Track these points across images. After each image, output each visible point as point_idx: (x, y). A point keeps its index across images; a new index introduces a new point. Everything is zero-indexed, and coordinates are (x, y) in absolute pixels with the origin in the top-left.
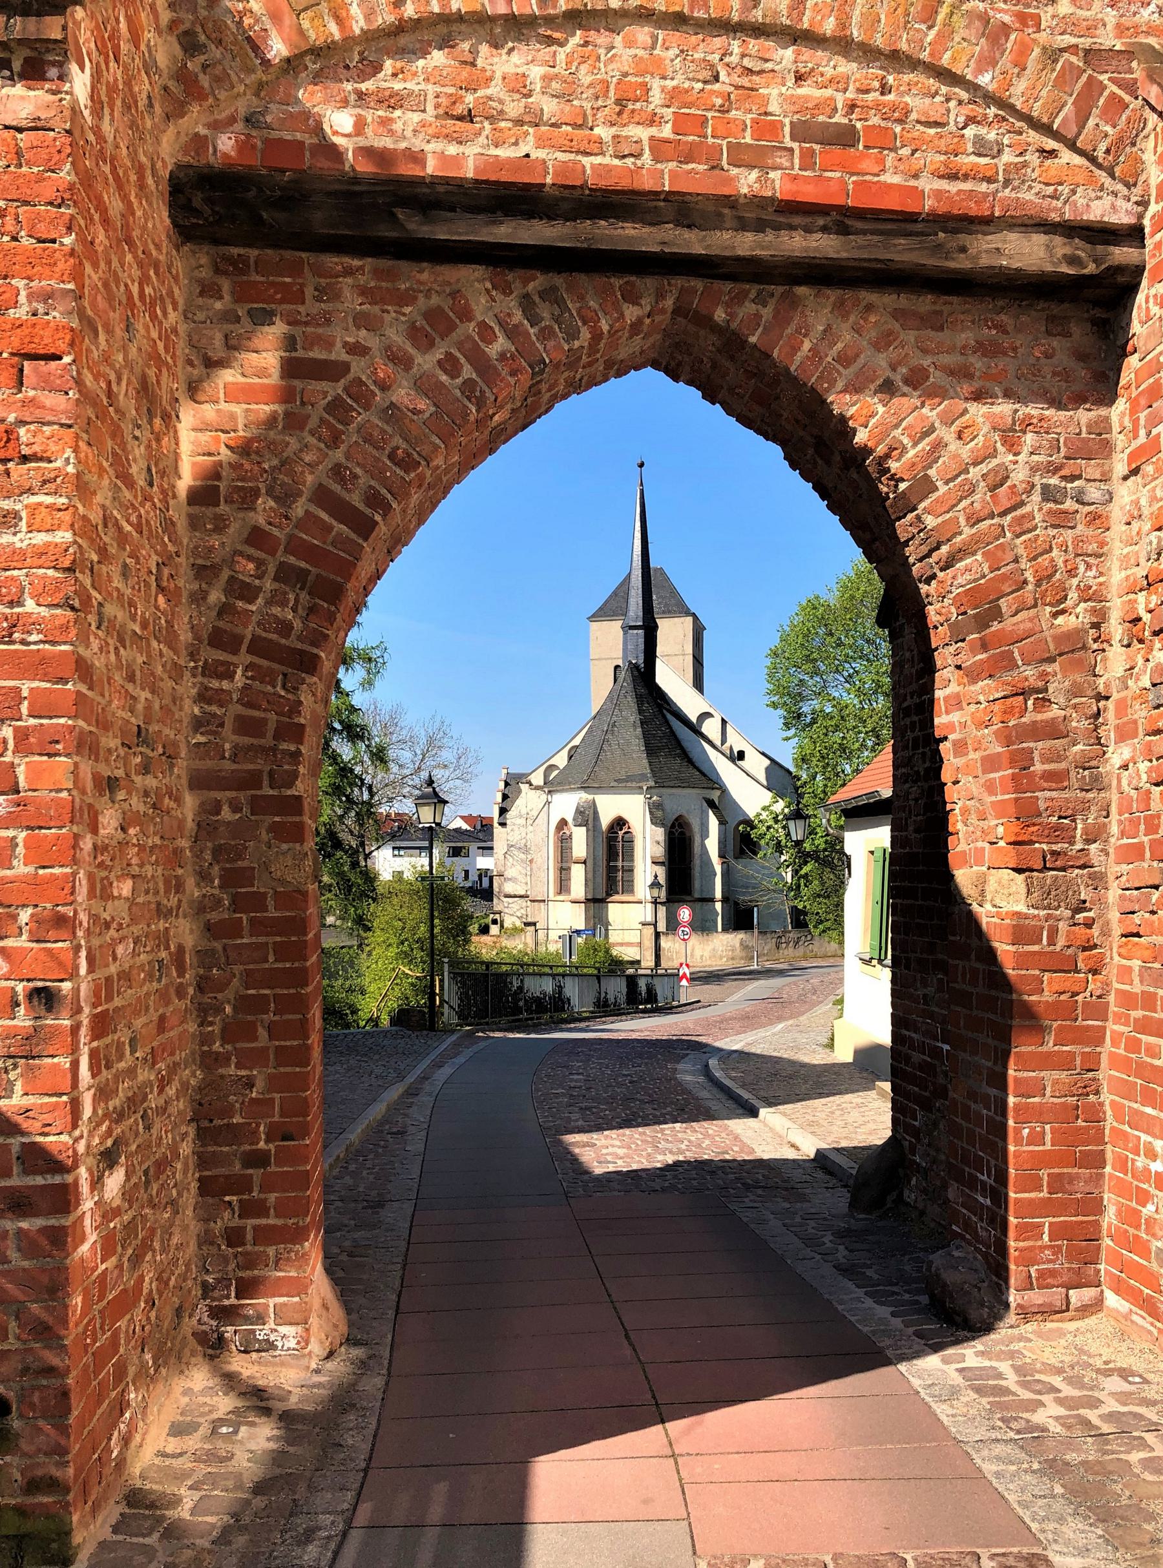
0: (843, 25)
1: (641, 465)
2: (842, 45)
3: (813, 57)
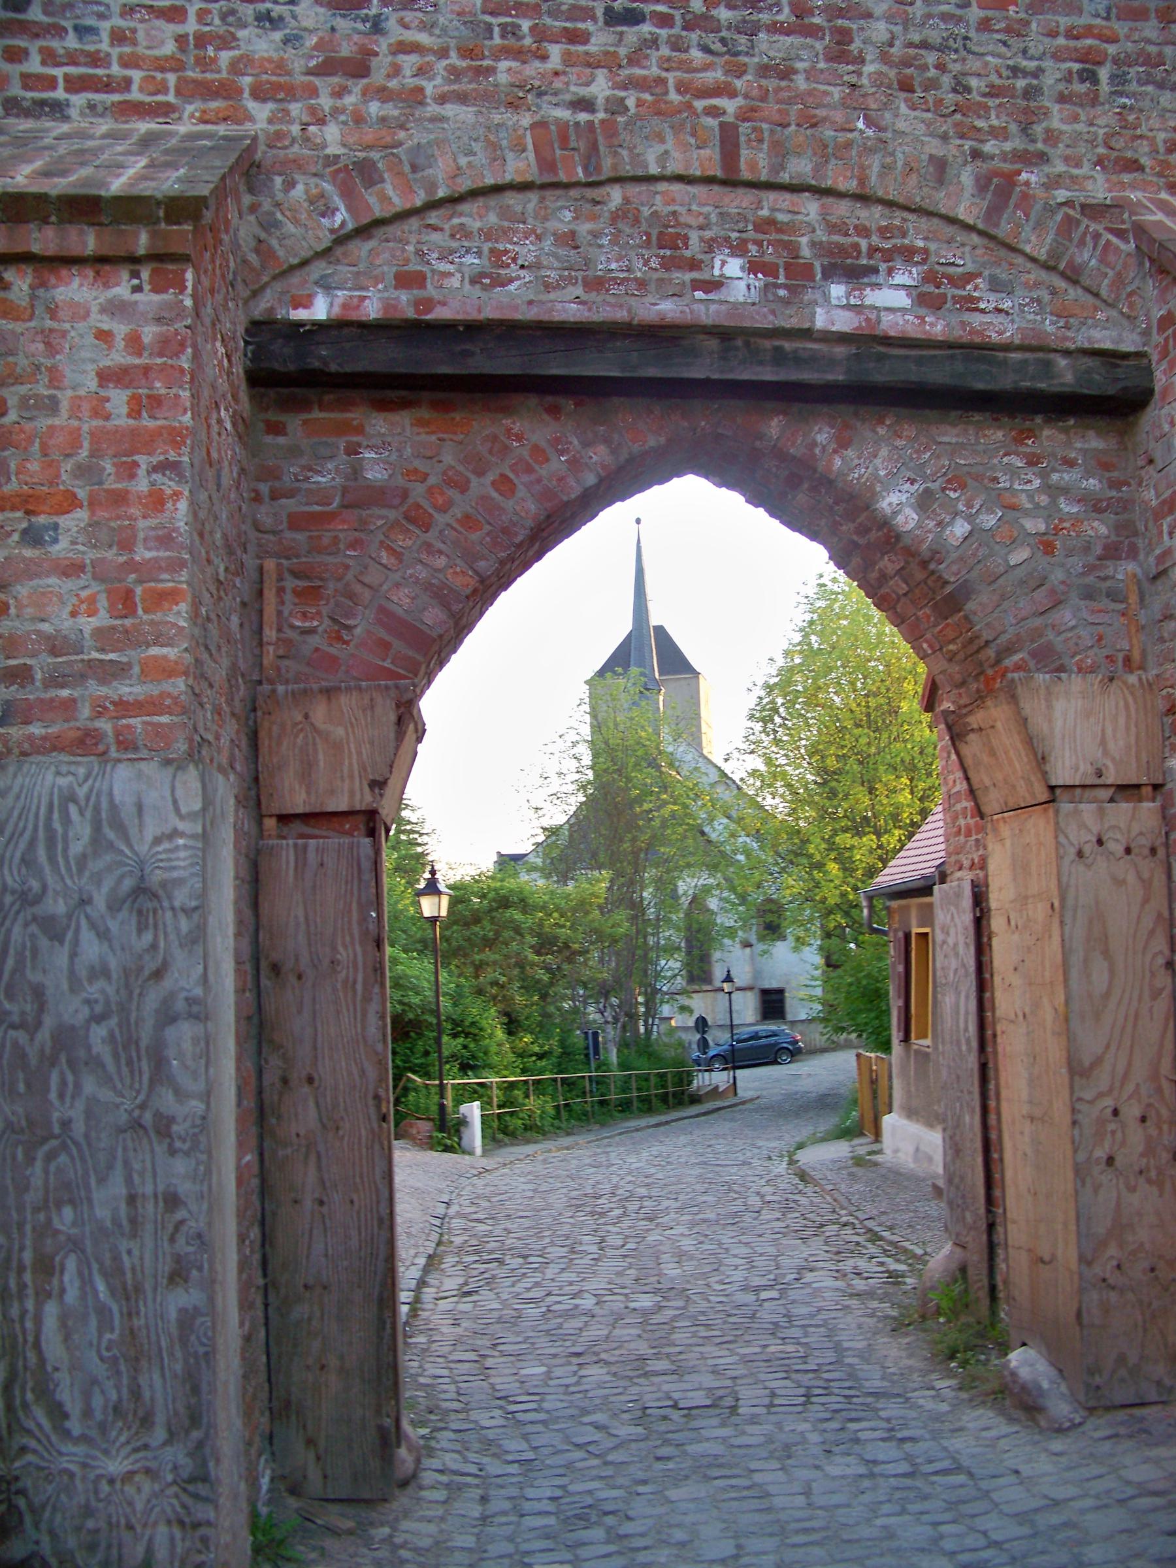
0: (862, 182)
1: (638, 521)
2: (863, 198)
3: (842, 209)
